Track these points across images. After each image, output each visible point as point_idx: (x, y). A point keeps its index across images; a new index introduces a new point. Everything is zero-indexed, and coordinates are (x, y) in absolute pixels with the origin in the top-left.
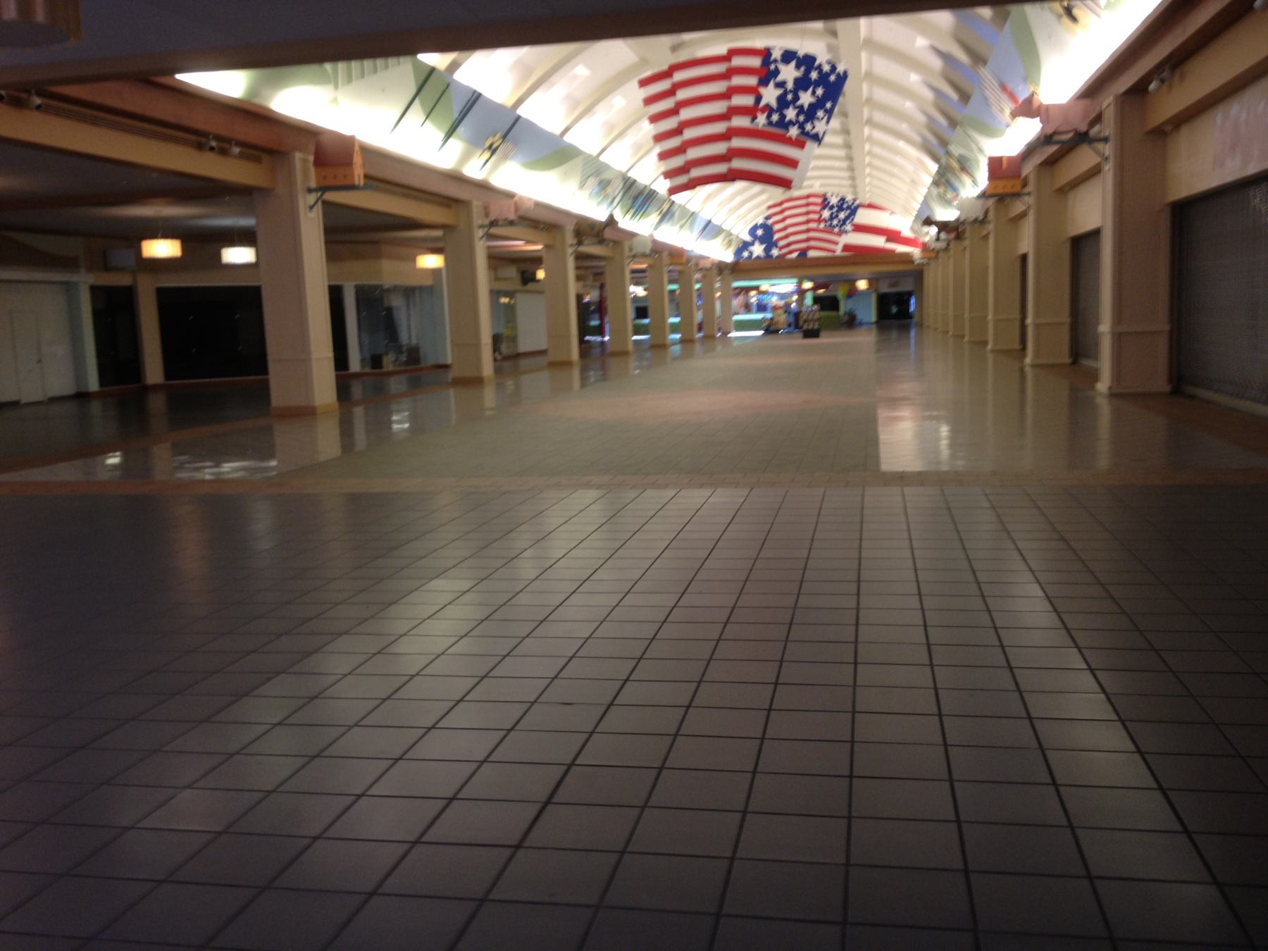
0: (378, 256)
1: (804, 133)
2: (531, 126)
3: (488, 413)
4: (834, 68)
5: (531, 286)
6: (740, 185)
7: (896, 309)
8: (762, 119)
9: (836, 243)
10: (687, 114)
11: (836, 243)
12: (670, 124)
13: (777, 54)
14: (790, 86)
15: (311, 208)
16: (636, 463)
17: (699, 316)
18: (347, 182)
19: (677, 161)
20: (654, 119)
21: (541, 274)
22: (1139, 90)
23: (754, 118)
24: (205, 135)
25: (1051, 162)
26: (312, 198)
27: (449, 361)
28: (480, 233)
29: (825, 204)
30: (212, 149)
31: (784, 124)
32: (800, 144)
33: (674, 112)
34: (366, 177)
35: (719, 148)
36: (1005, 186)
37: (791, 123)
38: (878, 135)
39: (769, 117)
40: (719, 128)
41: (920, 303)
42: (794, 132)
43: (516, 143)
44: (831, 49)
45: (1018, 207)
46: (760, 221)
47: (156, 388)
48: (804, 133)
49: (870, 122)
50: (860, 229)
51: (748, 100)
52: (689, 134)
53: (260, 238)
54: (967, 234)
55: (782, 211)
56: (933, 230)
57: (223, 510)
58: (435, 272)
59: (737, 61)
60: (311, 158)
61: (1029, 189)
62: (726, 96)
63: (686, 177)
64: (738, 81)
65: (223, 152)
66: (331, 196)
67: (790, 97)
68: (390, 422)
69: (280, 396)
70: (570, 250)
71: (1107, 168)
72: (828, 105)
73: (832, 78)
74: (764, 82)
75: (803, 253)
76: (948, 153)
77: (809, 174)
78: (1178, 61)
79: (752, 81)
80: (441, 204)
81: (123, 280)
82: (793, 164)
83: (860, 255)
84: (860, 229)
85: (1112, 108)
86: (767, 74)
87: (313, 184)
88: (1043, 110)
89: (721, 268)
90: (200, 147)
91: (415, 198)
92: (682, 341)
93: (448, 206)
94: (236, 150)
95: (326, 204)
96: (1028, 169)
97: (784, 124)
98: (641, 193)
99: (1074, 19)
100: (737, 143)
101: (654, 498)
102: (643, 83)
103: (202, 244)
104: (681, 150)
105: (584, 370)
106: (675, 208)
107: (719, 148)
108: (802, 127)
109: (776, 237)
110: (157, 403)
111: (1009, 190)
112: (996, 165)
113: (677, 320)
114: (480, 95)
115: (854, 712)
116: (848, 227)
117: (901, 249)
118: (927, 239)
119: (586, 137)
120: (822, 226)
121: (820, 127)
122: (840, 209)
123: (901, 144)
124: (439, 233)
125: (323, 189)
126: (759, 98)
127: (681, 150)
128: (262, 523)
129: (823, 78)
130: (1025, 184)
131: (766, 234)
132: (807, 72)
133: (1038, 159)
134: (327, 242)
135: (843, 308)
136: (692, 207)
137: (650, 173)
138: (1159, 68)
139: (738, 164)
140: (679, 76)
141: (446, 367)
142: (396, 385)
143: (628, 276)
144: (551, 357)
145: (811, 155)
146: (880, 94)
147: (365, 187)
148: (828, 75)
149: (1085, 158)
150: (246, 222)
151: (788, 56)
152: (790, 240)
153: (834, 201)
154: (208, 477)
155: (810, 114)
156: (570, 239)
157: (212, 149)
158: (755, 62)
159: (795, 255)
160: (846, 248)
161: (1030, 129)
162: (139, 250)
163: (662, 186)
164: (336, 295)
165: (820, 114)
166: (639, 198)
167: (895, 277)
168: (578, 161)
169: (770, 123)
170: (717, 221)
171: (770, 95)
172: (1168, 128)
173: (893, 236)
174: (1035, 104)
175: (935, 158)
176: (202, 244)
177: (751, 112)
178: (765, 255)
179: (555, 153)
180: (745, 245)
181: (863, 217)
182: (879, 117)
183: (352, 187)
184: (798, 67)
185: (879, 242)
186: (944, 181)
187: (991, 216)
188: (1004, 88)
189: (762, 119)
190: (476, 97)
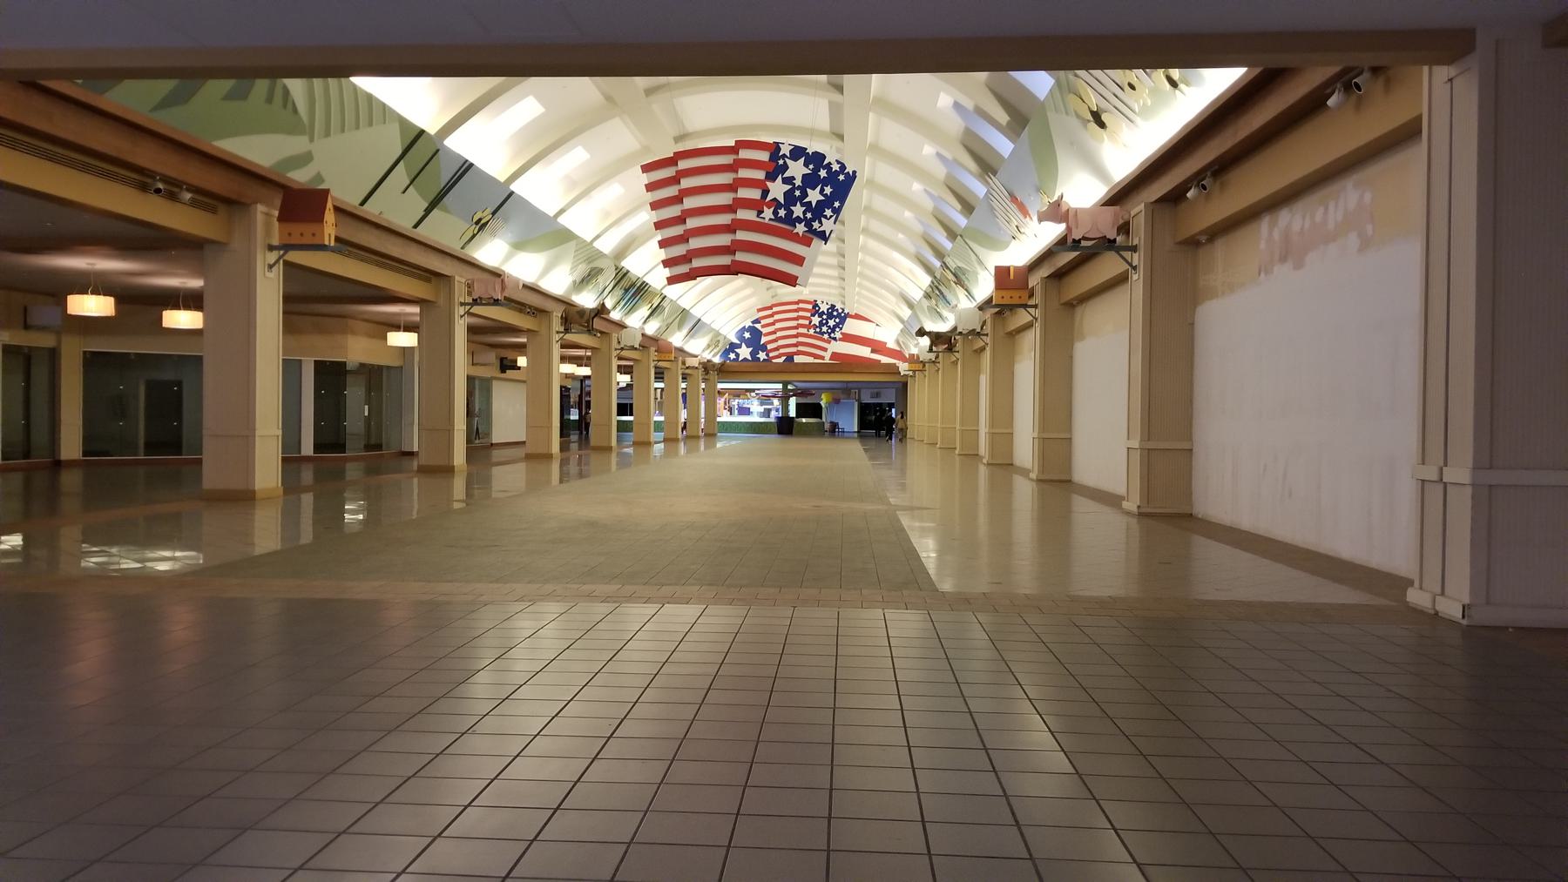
0: (344, 331)
1: (811, 230)
2: (524, 203)
3: (456, 506)
4: (843, 167)
5: (510, 373)
6: (742, 280)
7: (880, 422)
8: (768, 213)
9: (825, 350)
10: (690, 203)
11: (825, 350)
12: (673, 211)
13: (785, 150)
14: (798, 182)
15: (271, 267)
16: (643, 567)
17: (683, 415)
18: (316, 241)
19: (678, 250)
20: (655, 206)
21: (522, 361)
22: (1175, 197)
23: (760, 212)
24: (151, 174)
25: (1059, 275)
26: (272, 257)
27: (416, 449)
28: (462, 310)
29: (815, 309)
30: (158, 191)
31: (790, 220)
32: (807, 242)
33: (678, 200)
34: (338, 239)
35: (723, 240)
36: (1009, 297)
37: (799, 220)
38: (873, 244)
39: (775, 213)
40: (724, 219)
41: (903, 414)
42: (800, 229)
43: (506, 220)
44: (839, 150)
45: (1023, 317)
46: (748, 324)
47: (72, 464)
48: (811, 230)
49: (865, 231)
50: (848, 338)
51: (755, 194)
52: (692, 223)
53: (206, 302)
54: (959, 347)
55: (772, 316)
56: (925, 341)
57: (136, 604)
58: (405, 351)
59: (745, 154)
60: (276, 213)
61: (1036, 300)
62: (731, 188)
63: (684, 268)
64: (744, 173)
65: (172, 197)
66: (295, 257)
67: (797, 193)
68: (343, 511)
69: (213, 477)
70: (557, 337)
71: (1135, 277)
72: (837, 204)
73: (841, 177)
74: (771, 177)
75: (790, 358)
76: (945, 266)
77: (816, 270)
78: (1222, 167)
79: (760, 175)
80: (419, 278)
81: (45, 341)
82: (798, 260)
83: (844, 363)
84: (848, 338)
85: (1142, 218)
86: (775, 170)
87: (276, 242)
88: (1071, 214)
89: (707, 367)
90: (143, 188)
91: (392, 269)
92: (665, 440)
93: (428, 280)
94: (188, 196)
95: (288, 265)
96: (1034, 280)
97: (790, 220)
98: (633, 285)
99: (1102, 125)
100: (742, 235)
101: (637, 613)
102: (647, 168)
103: (141, 304)
104: (683, 239)
105: (564, 462)
106: (664, 304)
107: (723, 240)
108: (809, 224)
109: (764, 340)
110: (71, 481)
111: (1016, 301)
112: (1002, 274)
113: (662, 419)
114: (471, 165)
115: (829, 851)
116: (838, 335)
117: (885, 360)
118: (915, 351)
119: (582, 221)
120: (812, 331)
121: (827, 225)
122: (830, 316)
123: (896, 256)
124: (416, 309)
125: (287, 247)
126: (766, 192)
127: (683, 239)
128: (181, 624)
129: (832, 177)
130: (1031, 295)
131: (753, 337)
132: (816, 170)
133: (1045, 272)
134: (284, 313)
135: (826, 418)
136: (685, 303)
137: (647, 262)
138: (1197, 179)
139: (741, 257)
140: (684, 164)
141: (411, 454)
142: (353, 471)
143: (615, 368)
144: (529, 449)
145: (821, 256)
146: (880, 203)
147: (333, 250)
148: (837, 173)
149: (1109, 266)
150: (196, 283)
151: (797, 153)
152: (778, 342)
153: (824, 308)
154: (163, 567)
155: (818, 212)
156: (557, 325)
157: (158, 191)
158: (764, 156)
159: (781, 360)
160: (835, 355)
161: (1044, 234)
162: (63, 304)
163: (657, 278)
164: (291, 369)
165: (828, 212)
166: (635, 291)
167: (877, 388)
168: (572, 245)
169: (777, 218)
170: (722, 309)
171: (778, 190)
172: (1203, 239)
173: (877, 346)
174: (1064, 208)
175: (929, 270)
176: (141, 304)
177: (757, 206)
178: (744, 362)
179: (547, 233)
180: (733, 347)
181: (851, 327)
182: (875, 226)
183: (322, 247)
184: (806, 165)
185: (864, 352)
186: (936, 292)
187: (988, 329)
188: (1014, 199)
189: (768, 213)
190: (466, 167)
